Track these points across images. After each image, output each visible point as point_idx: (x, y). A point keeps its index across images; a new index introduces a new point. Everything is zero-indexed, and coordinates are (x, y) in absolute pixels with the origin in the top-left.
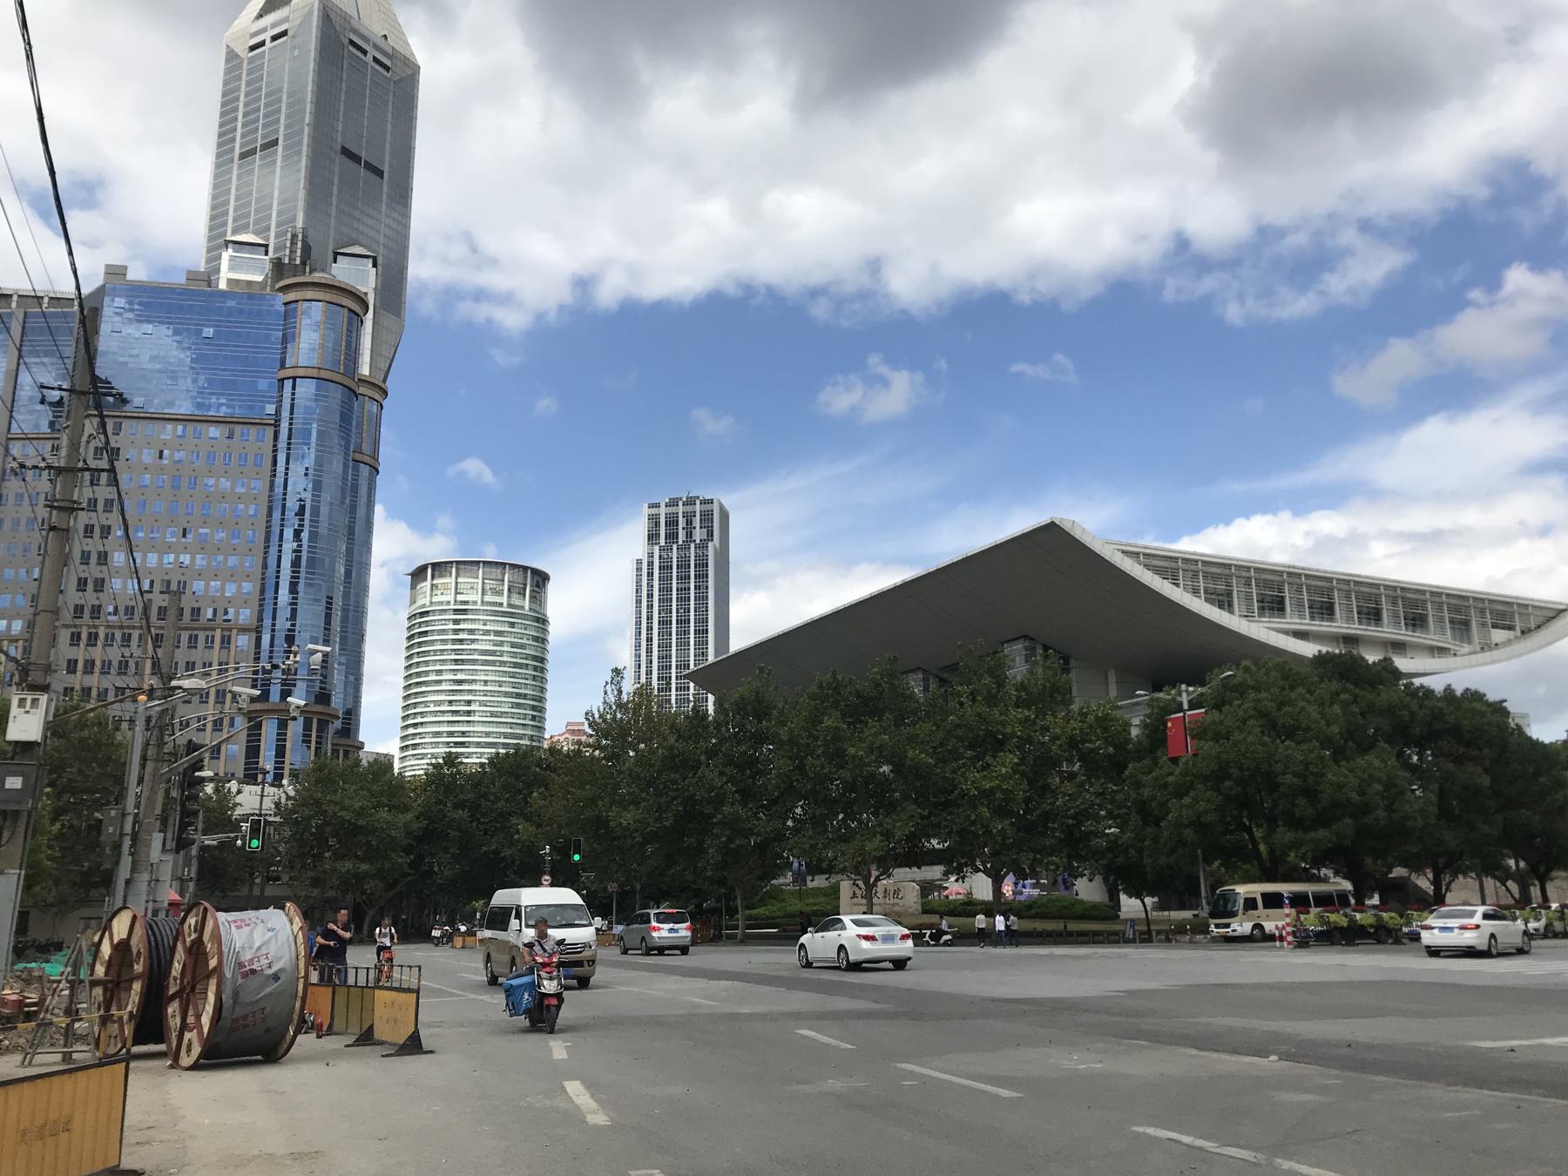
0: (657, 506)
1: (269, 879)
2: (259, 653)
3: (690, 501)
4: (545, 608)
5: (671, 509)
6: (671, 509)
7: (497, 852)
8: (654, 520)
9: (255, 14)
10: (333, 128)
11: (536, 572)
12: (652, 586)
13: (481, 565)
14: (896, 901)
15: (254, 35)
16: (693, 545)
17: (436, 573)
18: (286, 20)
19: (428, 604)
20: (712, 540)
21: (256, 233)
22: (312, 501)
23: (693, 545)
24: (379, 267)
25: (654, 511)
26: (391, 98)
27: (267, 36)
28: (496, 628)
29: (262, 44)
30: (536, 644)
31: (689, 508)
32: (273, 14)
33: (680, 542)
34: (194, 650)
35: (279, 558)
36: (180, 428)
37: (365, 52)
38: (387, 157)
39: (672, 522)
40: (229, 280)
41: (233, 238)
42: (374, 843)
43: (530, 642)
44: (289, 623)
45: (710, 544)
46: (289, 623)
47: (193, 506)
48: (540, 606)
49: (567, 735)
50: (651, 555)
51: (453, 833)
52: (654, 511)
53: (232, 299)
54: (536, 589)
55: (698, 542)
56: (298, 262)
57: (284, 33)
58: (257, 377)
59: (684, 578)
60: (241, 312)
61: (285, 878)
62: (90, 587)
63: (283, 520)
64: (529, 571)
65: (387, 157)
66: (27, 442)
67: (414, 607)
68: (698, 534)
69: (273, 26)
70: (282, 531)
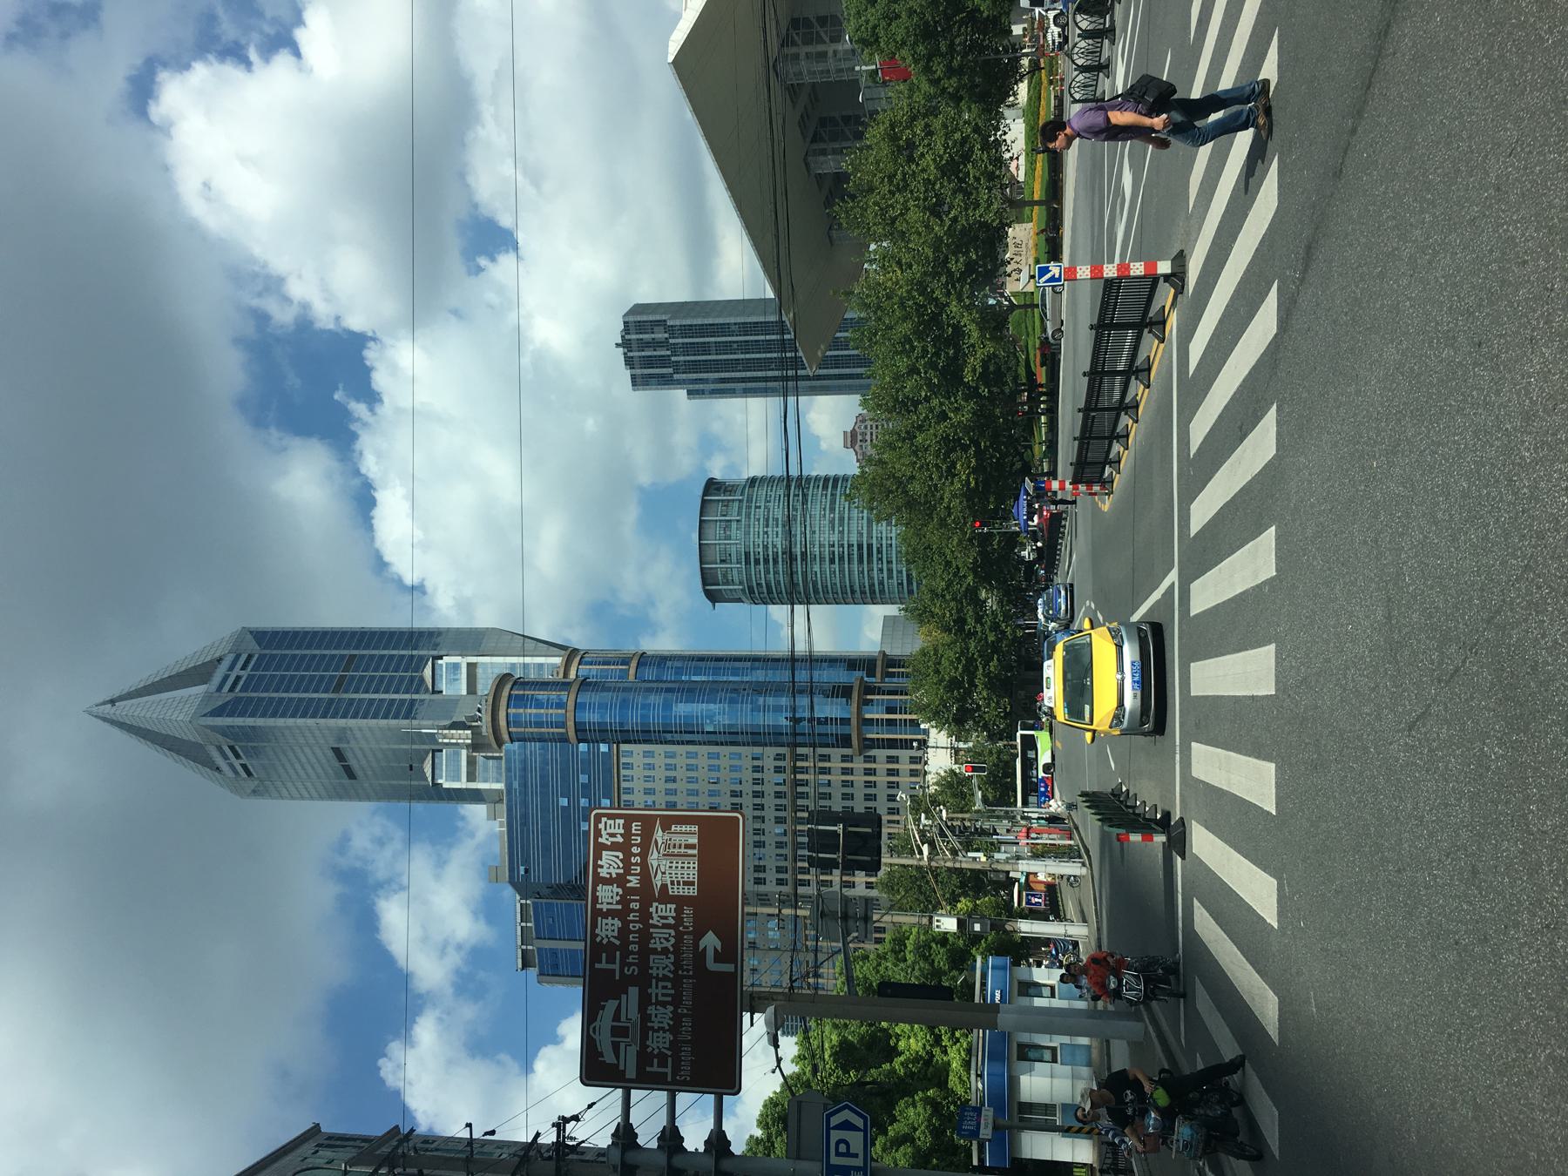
11: (706, 491)
14: (1024, 245)
15: (236, 772)
16: (671, 341)
18: (220, 749)
20: (665, 321)
21: (423, 761)
23: (671, 341)
24: (441, 653)
27: (237, 763)
29: (244, 767)
31: (634, 346)
33: (669, 353)
37: (238, 678)
39: (648, 362)
40: (468, 781)
41: (430, 779)
45: (670, 323)
49: (857, 447)
55: (667, 335)
56: (469, 732)
57: (232, 748)
59: (704, 349)
62: (761, 875)
68: (660, 336)
69: (226, 757)
70: (708, 733)
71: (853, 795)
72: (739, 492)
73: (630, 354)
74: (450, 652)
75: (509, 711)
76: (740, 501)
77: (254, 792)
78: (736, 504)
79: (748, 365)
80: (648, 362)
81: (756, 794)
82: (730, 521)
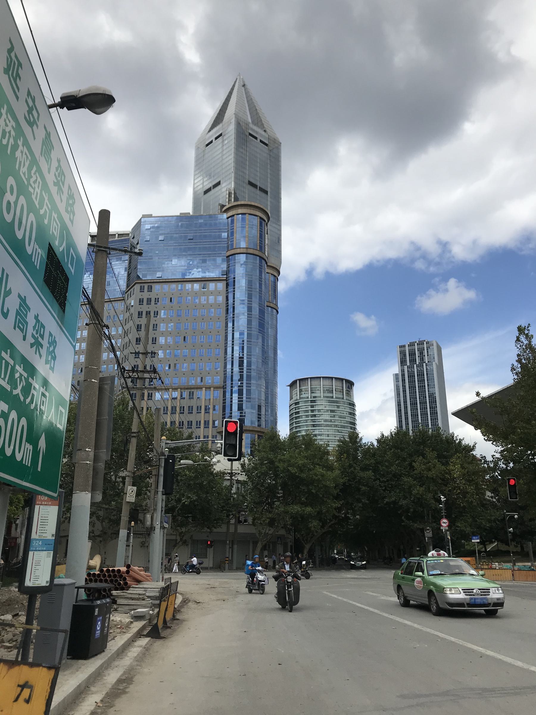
0: (404, 346)
1: (240, 522)
2: (225, 400)
3: (421, 343)
4: (353, 399)
5: (411, 348)
6: (411, 348)
7: (394, 503)
8: (403, 354)
9: (208, 131)
10: (244, 173)
12: (405, 386)
13: (322, 378)
15: (209, 138)
17: (301, 384)
19: (298, 398)
22: (248, 330)
25: (403, 349)
26: (269, 167)
27: (213, 138)
28: (331, 409)
30: (350, 416)
32: (215, 128)
33: (418, 363)
34: (192, 400)
35: (231, 405)
36: (180, 286)
38: (269, 185)
39: (412, 354)
42: (314, 491)
43: (347, 415)
44: (239, 382)
46: (239, 382)
47: (188, 325)
48: (351, 398)
50: (403, 371)
51: (363, 488)
52: (403, 349)
53: (201, 218)
54: (348, 389)
58: (216, 256)
60: (206, 224)
61: (250, 520)
63: (232, 384)
64: (344, 381)
65: (269, 185)
66: (109, 303)
67: (292, 401)
71: (192, 413)
72: (348, 398)
73: (416, 344)
74: (269, 240)
75: (247, 215)
76: (343, 398)
77: (198, 148)
78: (341, 396)
79: (414, 404)
80: (412, 354)
81: (190, 408)
82: (333, 393)
